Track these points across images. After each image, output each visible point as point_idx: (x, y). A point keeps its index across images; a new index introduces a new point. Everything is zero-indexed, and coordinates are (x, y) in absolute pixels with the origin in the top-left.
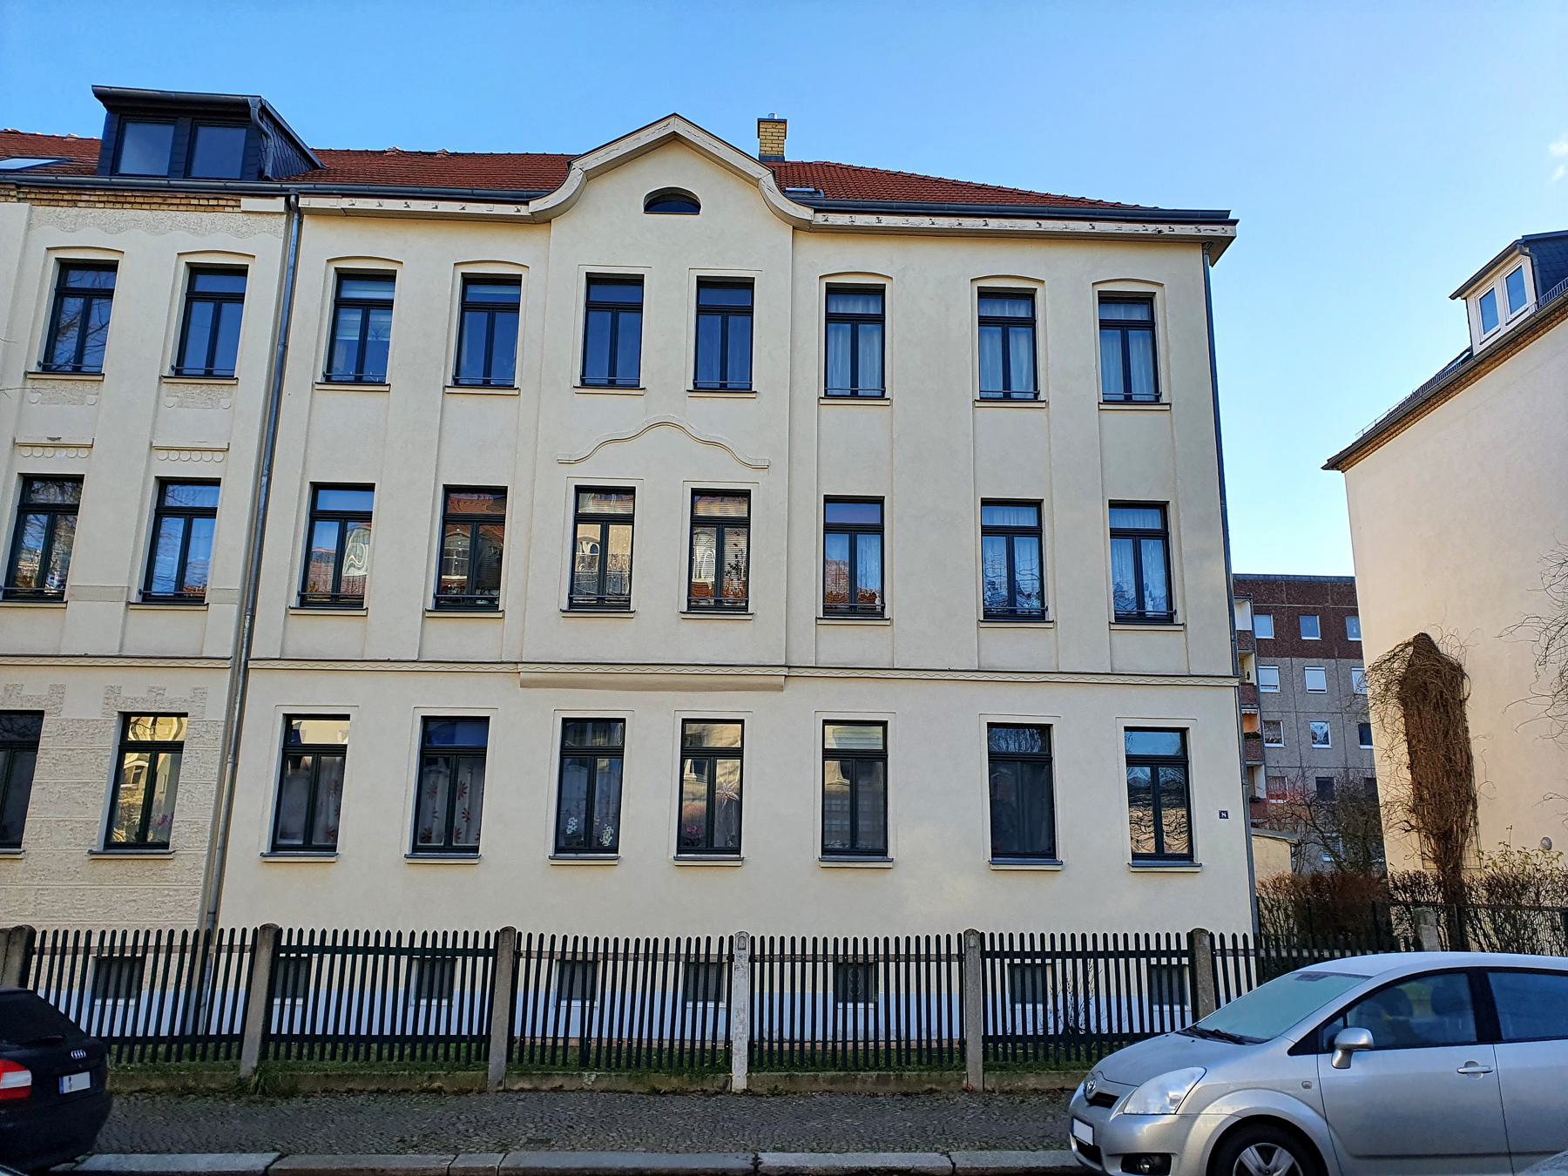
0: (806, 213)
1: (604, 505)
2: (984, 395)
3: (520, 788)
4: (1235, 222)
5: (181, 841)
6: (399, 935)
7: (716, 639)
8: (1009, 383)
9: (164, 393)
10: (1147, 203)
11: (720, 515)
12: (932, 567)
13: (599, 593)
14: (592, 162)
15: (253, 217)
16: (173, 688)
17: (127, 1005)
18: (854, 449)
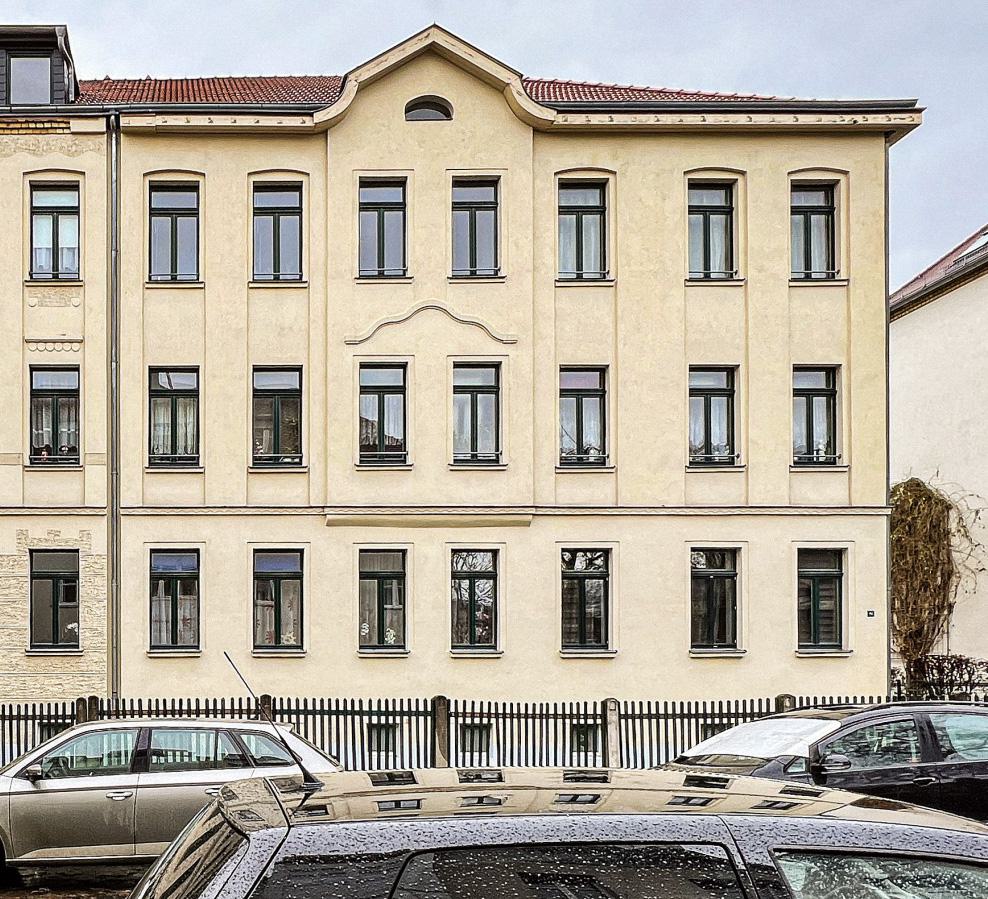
0: (549, 115)
1: (385, 383)
2: (456, 273)
3: (332, 598)
4: (920, 111)
5: (87, 643)
6: (223, 701)
7: (477, 488)
8: (716, 269)
9: (26, 295)
10: (783, 95)
11: (480, 385)
12: (651, 425)
13: (381, 451)
14: (365, 75)
15: (80, 137)
16: (65, 533)
17: (379, 756)
18: (583, 326)
